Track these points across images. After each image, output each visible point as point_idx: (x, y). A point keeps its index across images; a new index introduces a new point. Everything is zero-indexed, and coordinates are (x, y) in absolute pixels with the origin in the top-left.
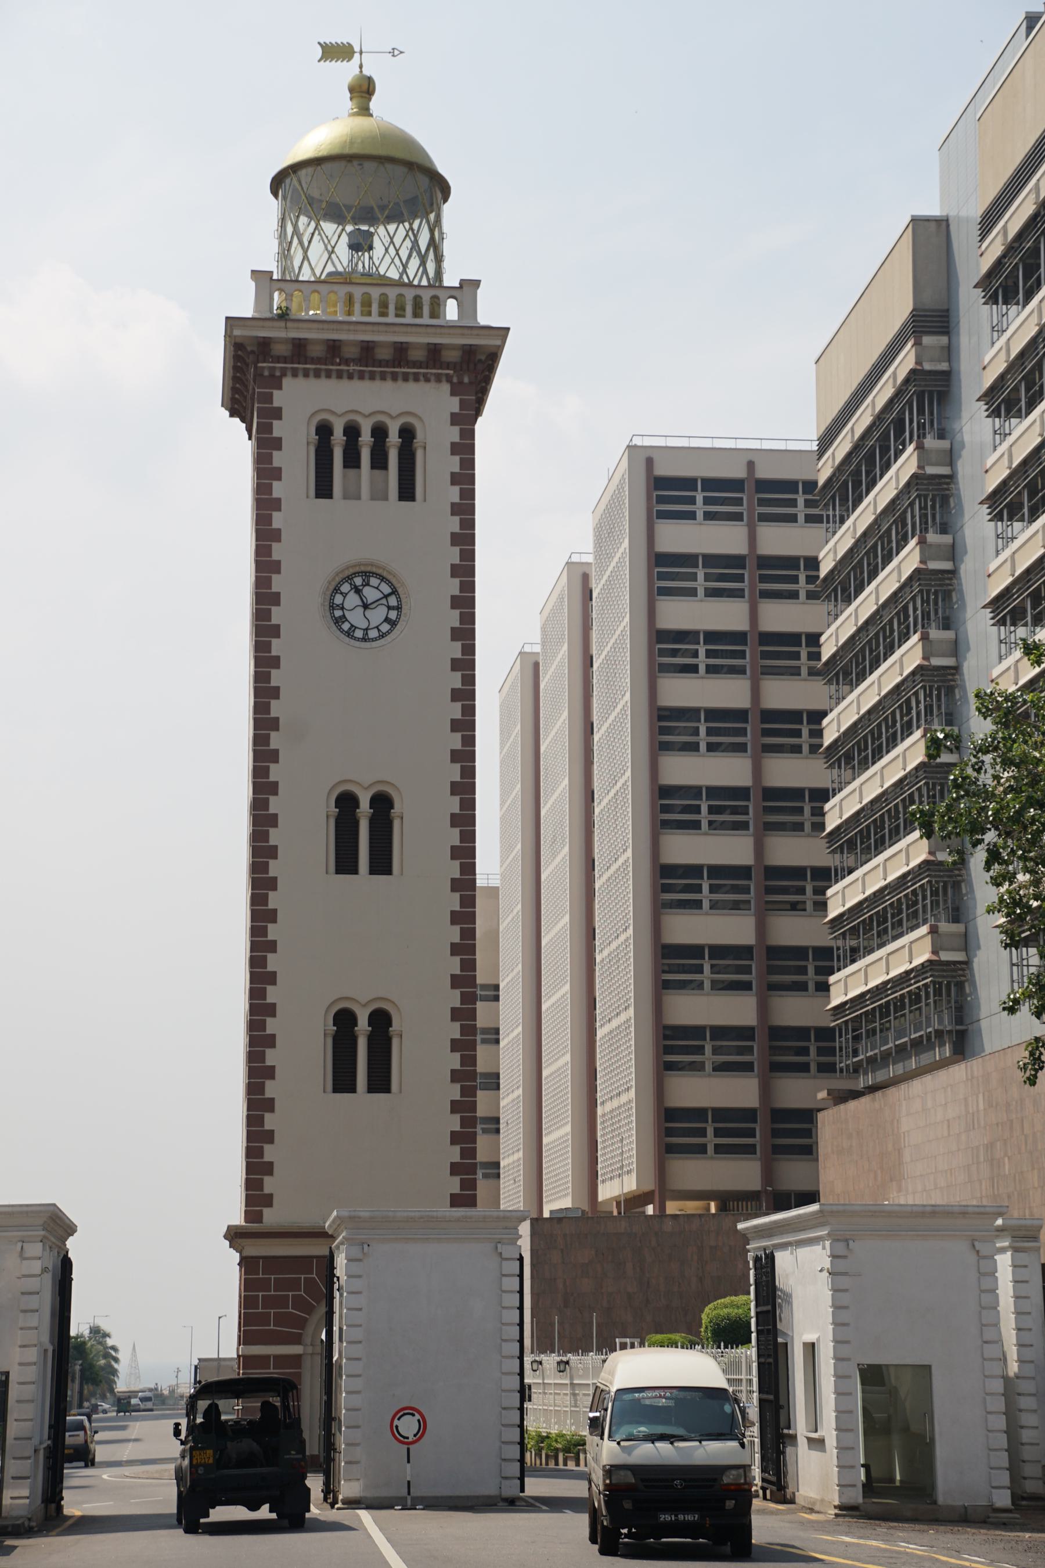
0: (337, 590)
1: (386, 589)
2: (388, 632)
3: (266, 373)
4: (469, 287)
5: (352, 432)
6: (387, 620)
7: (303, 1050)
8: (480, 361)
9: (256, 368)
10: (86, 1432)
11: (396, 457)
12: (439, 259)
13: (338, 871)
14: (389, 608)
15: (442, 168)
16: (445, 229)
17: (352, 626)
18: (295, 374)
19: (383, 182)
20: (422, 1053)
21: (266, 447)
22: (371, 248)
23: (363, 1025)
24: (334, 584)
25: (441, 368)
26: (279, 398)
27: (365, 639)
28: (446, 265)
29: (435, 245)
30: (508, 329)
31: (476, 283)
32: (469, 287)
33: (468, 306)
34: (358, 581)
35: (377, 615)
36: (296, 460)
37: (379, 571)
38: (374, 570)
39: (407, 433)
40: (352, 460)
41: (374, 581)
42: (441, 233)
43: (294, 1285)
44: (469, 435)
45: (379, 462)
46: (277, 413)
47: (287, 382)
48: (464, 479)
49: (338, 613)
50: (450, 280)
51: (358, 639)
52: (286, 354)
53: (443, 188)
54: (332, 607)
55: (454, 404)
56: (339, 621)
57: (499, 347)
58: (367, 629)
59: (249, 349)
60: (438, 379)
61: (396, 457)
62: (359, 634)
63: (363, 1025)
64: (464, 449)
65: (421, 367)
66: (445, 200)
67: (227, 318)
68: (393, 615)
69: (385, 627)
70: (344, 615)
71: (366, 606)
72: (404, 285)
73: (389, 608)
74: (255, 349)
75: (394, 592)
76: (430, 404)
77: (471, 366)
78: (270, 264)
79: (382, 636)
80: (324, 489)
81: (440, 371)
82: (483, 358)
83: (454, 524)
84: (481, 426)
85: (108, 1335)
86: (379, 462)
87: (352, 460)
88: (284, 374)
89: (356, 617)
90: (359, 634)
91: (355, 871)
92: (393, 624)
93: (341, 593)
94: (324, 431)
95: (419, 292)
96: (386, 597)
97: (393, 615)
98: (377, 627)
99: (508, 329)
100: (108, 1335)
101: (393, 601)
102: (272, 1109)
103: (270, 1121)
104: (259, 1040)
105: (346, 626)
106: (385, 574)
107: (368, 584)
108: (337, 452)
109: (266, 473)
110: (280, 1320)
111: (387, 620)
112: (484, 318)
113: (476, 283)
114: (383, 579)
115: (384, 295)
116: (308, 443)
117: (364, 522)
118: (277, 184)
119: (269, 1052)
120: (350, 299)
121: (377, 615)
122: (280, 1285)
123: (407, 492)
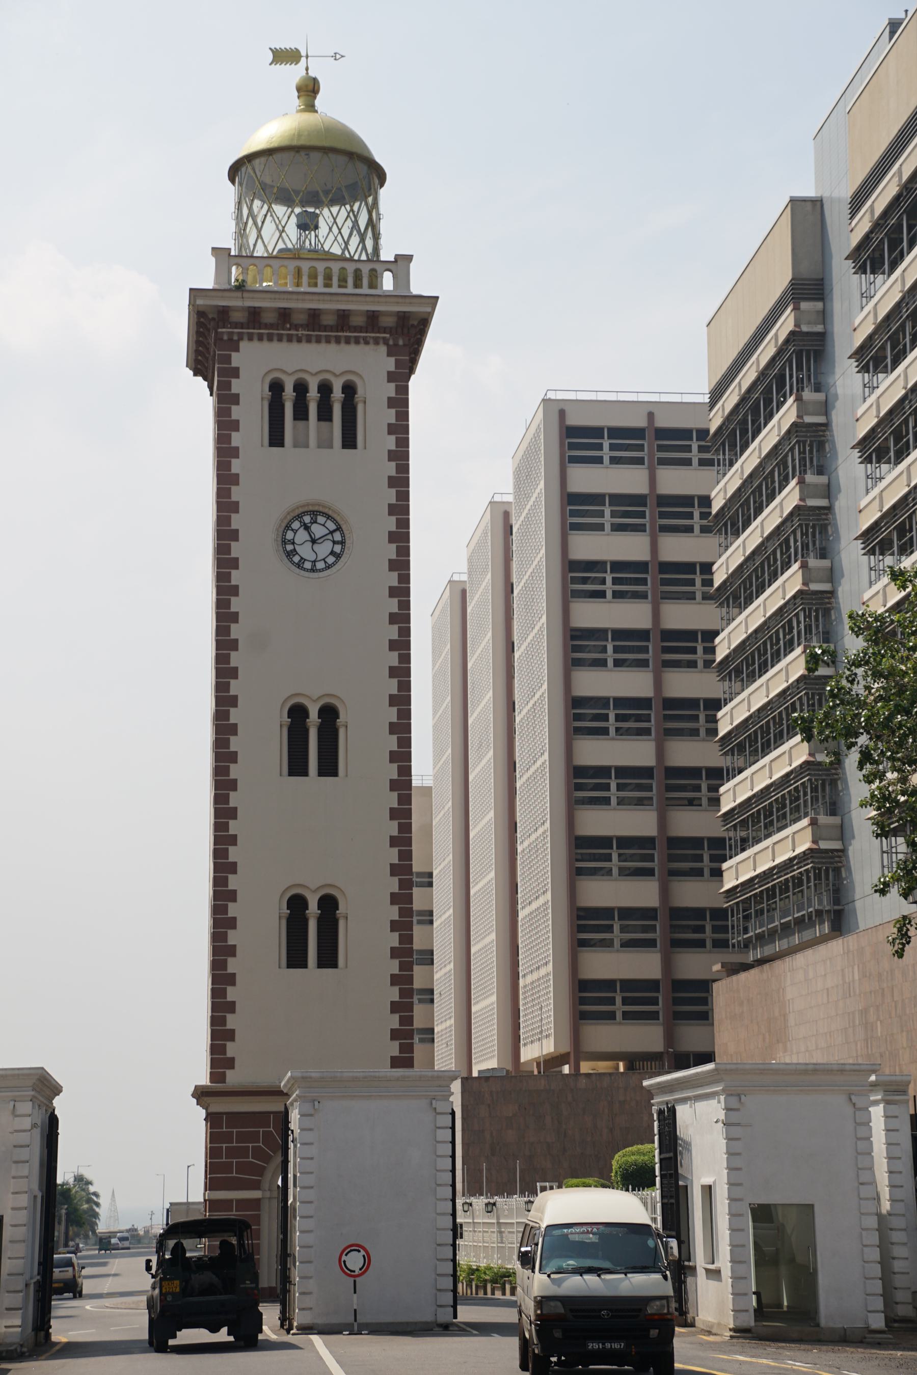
0: (288, 527)
1: (331, 526)
2: (334, 564)
3: (225, 338)
4: (403, 261)
5: (301, 388)
6: (332, 553)
7: (262, 741)
8: (413, 325)
9: (216, 333)
10: (74, 1268)
11: (340, 410)
12: (376, 237)
13: (291, 774)
14: (334, 542)
15: (378, 159)
16: (382, 211)
17: (302, 558)
18: (250, 339)
19: (326, 170)
20: (366, 933)
21: (226, 402)
22: (316, 227)
23: (313, 908)
24: (286, 522)
25: (379, 332)
26: (236, 359)
27: (313, 570)
28: (382, 242)
29: (373, 224)
30: (437, 298)
31: (409, 258)
32: (403, 261)
33: (402, 278)
34: (307, 519)
35: (324, 549)
36: (252, 414)
37: (326, 511)
38: (321, 509)
39: (349, 390)
40: (301, 413)
41: (321, 519)
42: (378, 214)
43: (254, 1137)
44: (403, 391)
45: (325, 414)
46: (235, 373)
47: (243, 345)
48: (400, 429)
49: (289, 547)
50: (387, 255)
51: (307, 570)
52: (242, 320)
53: (378, 174)
54: (284, 542)
55: (390, 364)
56: (290, 554)
57: (429, 313)
58: (315, 561)
59: (210, 316)
60: (376, 342)
61: (340, 410)
62: (308, 565)
63: (313, 908)
64: (400, 403)
65: (361, 332)
66: (382, 185)
67: (191, 290)
68: (338, 549)
69: (331, 560)
70: (295, 549)
71: (314, 541)
72: (346, 259)
73: (334, 542)
74: (215, 316)
75: (339, 528)
76: (369, 364)
77: (405, 330)
78: (229, 242)
79: (328, 567)
80: (276, 439)
81: (378, 335)
82: (415, 323)
83: (391, 469)
84: (414, 383)
85: (91, 1183)
86: (325, 414)
87: (301, 413)
88: (241, 338)
89: (305, 551)
90: (308, 565)
91: (304, 965)
92: (338, 556)
93: (292, 530)
94: (276, 388)
95: (359, 266)
96: (331, 533)
97: (338, 549)
98: (324, 559)
99: (437, 298)
100: (91, 1183)
101: (337, 536)
102: (233, 983)
103: (233, 910)
104: (222, 922)
105: (296, 559)
106: (330, 513)
107: (315, 522)
108: (287, 407)
109: (225, 425)
110: (241, 1168)
111: (332, 553)
112: (416, 289)
113: (409, 258)
114: (328, 517)
115: (343, 269)
116: (280, 918)
117: (311, 467)
118: (234, 171)
119: (231, 933)
120: (299, 272)
121: (324, 549)
122: (242, 1137)
123: (349, 441)
